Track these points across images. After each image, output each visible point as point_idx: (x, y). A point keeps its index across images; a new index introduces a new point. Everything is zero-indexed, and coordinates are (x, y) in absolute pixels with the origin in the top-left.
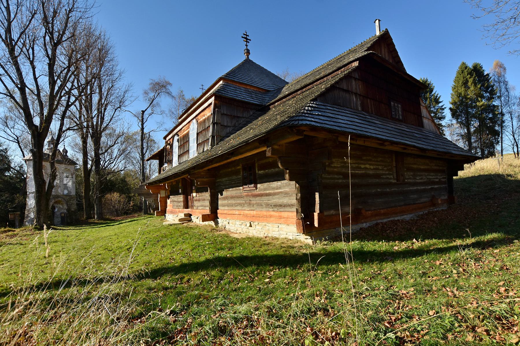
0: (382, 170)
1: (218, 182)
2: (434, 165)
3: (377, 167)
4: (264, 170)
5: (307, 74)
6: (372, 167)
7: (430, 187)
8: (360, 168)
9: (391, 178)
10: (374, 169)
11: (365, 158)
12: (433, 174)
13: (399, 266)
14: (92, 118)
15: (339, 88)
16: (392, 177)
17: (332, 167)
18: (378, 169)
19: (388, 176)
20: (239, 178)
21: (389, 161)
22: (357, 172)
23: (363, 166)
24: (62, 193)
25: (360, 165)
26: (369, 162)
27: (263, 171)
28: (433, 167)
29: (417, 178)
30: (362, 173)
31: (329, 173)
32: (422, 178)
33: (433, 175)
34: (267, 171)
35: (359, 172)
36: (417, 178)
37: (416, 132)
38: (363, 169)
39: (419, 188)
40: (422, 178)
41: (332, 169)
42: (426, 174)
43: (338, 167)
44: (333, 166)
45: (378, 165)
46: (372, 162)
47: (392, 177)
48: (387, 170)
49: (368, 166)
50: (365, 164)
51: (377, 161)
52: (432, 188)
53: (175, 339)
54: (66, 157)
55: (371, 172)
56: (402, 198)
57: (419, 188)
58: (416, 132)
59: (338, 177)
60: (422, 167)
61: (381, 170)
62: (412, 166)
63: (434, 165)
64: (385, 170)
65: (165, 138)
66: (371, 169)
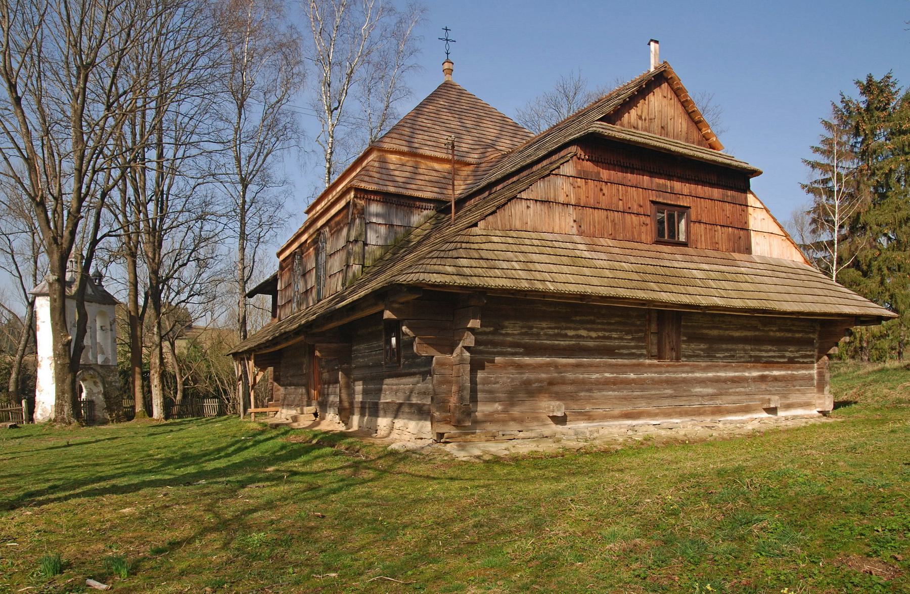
0: (621, 339)
1: (355, 351)
5: (628, 84)
6: (594, 334)
7: (755, 374)
8: (566, 336)
9: (752, 350)
11: (578, 318)
12: (769, 347)
14: (145, 205)
17: (502, 334)
18: (609, 338)
19: (633, 351)
20: (379, 346)
21: (638, 323)
22: (556, 342)
23: (571, 333)
24: (94, 362)
26: (585, 326)
28: (772, 334)
29: (718, 355)
30: (569, 346)
32: (733, 356)
33: (770, 351)
35: (562, 343)
40: (733, 356)
41: (501, 338)
43: (513, 334)
44: (504, 332)
45: (610, 331)
46: (595, 326)
49: (583, 333)
50: (576, 329)
51: (610, 324)
52: (763, 378)
54: (100, 288)
55: (591, 344)
59: (513, 351)
61: (615, 339)
65: (279, 255)
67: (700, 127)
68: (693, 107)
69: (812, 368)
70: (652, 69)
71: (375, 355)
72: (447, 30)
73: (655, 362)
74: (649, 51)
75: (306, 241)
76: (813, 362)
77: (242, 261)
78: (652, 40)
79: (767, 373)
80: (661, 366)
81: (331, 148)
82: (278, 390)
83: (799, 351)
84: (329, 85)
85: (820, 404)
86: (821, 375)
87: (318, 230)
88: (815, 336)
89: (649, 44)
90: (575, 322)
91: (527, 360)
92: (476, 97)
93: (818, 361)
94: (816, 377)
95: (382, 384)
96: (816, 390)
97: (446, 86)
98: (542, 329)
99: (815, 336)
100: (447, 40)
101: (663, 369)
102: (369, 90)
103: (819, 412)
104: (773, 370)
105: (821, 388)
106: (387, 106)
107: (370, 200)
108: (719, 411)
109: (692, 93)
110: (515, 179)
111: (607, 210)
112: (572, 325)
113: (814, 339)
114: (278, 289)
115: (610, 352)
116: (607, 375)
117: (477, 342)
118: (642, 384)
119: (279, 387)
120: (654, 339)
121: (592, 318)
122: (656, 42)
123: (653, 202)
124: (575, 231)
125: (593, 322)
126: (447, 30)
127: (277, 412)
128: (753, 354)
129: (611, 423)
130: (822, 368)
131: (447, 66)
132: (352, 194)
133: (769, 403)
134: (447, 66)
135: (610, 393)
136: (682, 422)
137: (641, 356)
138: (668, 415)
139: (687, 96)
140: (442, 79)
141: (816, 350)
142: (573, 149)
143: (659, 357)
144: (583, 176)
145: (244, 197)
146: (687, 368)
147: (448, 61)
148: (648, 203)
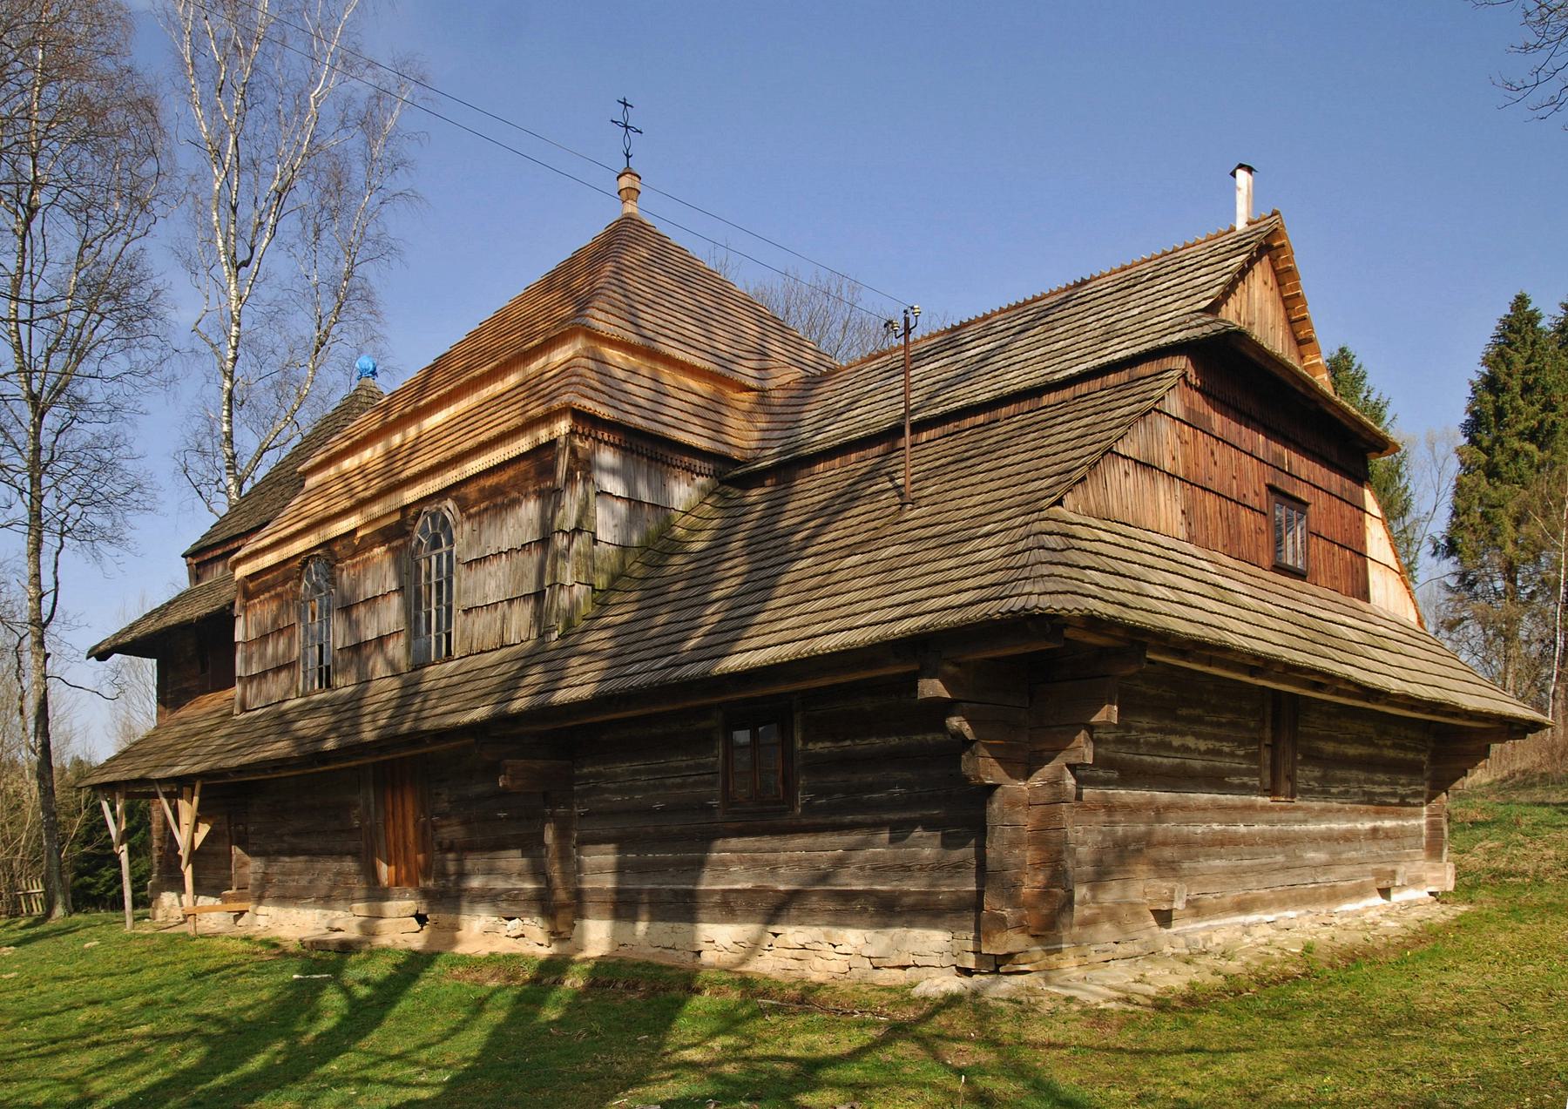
0: (1232, 755)
2: (1389, 743)
3: (1218, 744)
4: (834, 737)
8: (1169, 747)
10: (1209, 752)
13: (1238, 1055)
15: (1160, 412)
16: (1257, 783)
18: (1218, 753)
19: (1246, 779)
21: (1252, 724)
23: (1176, 741)
25: (1169, 738)
26: (1197, 728)
27: (828, 744)
29: (1333, 790)
31: (41, 392)
34: (848, 743)
36: (1333, 790)
37: (1349, 621)
38: (1177, 750)
39: (1334, 826)
42: (1362, 776)
47: (1257, 783)
48: (1243, 757)
49: (1190, 741)
50: (1182, 734)
51: (1219, 725)
52: (1375, 830)
53: (195, 562)
55: (1198, 764)
56: (1280, 858)
57: (1334, 826)
58: (1349, 621)
60: (1352, 751)
62: (1321, 744)
63: (1389, 743)
64: (1238, 756)
66: (1197, 750)
67: (1304, 352)
68: (1304, 309)
69: (1417, 816)
70: (1241, 225)
71: (695, 784)
72: (626, 105)
73: (1267, 800)
74: (1234, 189)
75: (354, 532)
76: (1421, 805)
77: (34, 581)
78: (1241, 166)
79: (1378, 823)
80: (1272, 809)
81: (235, 348)
82: (245, 864)
83: (1410, 784)
84: (234, 209)
85: (1435, 879)
86: (1434, 827)
87: (404, 509)
88: (1424, 758)
89: (1233, 174)
90: (1177, 719)
91: (1123, 794)
92: (691, 254)
93: (1429, 801)
94: (1425, 831)
95: (708, 850)
96: (1423, 854)
97: (624, 233)
98: (1143, 731)
99: (1424, 758)
100: (627, 127)
101: (1275, 816)
102: (317, 233)
103: (1431, 894)
104: (1385, 818)
105: (1434, 850)
106: (350, 272)
107: (600, 441)
108: (1335, 895)
109: (1308, 285)
110: (981, 419)
111: (1219, 495)
112: (1178, 726)
113: (1423, 763)
114: (239, 636)
115: (1215, 781)
116: (1215, 826)
117: (1099, 761)
118: (1252, 845)
119: (247, 858)
120: (1266, 755)
121: (1199, 711)
122: (1250, 170)
123: (1271, 488)
124: (1182, 534)
125: (1199, 720)
126: (626, 105)
127: (242, 913)
128: (1367, 788)
129: (1222, 922)
130: (1439, 815)
131: (625, 182)
132: (563, 426)
133: (1394, 879)
134: (625, 182)
135: (1217, 862)
136: (1298, 917)
137: (1250, 790)
138: (1282, 903)
139: (1297, 286)
140: (614, 211)
141: (1426, 783)
142: (1181, 363)
143: (1272, 791)
144: (1192, 422)
145: (37, 435)
146: (1300, 815)
147: (628, 171)
148: (1264, 489)
